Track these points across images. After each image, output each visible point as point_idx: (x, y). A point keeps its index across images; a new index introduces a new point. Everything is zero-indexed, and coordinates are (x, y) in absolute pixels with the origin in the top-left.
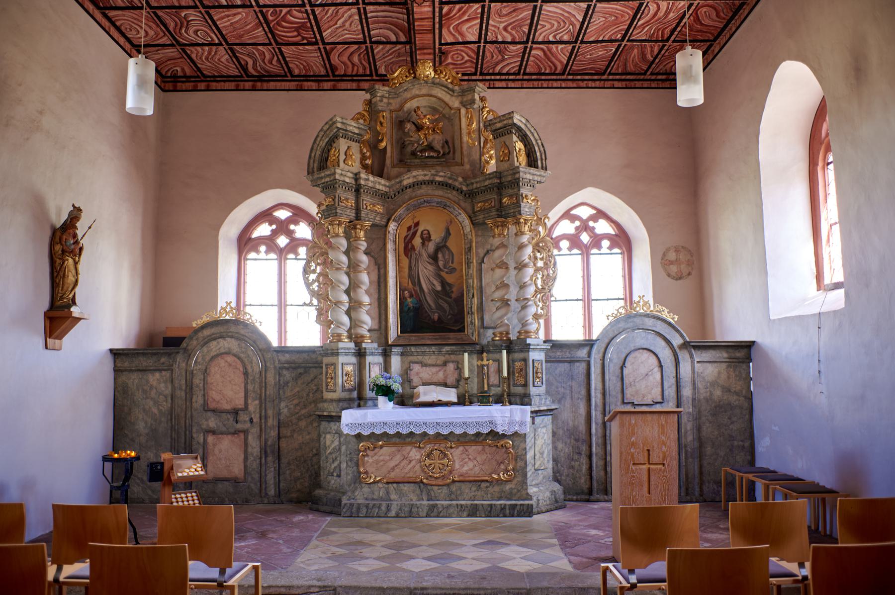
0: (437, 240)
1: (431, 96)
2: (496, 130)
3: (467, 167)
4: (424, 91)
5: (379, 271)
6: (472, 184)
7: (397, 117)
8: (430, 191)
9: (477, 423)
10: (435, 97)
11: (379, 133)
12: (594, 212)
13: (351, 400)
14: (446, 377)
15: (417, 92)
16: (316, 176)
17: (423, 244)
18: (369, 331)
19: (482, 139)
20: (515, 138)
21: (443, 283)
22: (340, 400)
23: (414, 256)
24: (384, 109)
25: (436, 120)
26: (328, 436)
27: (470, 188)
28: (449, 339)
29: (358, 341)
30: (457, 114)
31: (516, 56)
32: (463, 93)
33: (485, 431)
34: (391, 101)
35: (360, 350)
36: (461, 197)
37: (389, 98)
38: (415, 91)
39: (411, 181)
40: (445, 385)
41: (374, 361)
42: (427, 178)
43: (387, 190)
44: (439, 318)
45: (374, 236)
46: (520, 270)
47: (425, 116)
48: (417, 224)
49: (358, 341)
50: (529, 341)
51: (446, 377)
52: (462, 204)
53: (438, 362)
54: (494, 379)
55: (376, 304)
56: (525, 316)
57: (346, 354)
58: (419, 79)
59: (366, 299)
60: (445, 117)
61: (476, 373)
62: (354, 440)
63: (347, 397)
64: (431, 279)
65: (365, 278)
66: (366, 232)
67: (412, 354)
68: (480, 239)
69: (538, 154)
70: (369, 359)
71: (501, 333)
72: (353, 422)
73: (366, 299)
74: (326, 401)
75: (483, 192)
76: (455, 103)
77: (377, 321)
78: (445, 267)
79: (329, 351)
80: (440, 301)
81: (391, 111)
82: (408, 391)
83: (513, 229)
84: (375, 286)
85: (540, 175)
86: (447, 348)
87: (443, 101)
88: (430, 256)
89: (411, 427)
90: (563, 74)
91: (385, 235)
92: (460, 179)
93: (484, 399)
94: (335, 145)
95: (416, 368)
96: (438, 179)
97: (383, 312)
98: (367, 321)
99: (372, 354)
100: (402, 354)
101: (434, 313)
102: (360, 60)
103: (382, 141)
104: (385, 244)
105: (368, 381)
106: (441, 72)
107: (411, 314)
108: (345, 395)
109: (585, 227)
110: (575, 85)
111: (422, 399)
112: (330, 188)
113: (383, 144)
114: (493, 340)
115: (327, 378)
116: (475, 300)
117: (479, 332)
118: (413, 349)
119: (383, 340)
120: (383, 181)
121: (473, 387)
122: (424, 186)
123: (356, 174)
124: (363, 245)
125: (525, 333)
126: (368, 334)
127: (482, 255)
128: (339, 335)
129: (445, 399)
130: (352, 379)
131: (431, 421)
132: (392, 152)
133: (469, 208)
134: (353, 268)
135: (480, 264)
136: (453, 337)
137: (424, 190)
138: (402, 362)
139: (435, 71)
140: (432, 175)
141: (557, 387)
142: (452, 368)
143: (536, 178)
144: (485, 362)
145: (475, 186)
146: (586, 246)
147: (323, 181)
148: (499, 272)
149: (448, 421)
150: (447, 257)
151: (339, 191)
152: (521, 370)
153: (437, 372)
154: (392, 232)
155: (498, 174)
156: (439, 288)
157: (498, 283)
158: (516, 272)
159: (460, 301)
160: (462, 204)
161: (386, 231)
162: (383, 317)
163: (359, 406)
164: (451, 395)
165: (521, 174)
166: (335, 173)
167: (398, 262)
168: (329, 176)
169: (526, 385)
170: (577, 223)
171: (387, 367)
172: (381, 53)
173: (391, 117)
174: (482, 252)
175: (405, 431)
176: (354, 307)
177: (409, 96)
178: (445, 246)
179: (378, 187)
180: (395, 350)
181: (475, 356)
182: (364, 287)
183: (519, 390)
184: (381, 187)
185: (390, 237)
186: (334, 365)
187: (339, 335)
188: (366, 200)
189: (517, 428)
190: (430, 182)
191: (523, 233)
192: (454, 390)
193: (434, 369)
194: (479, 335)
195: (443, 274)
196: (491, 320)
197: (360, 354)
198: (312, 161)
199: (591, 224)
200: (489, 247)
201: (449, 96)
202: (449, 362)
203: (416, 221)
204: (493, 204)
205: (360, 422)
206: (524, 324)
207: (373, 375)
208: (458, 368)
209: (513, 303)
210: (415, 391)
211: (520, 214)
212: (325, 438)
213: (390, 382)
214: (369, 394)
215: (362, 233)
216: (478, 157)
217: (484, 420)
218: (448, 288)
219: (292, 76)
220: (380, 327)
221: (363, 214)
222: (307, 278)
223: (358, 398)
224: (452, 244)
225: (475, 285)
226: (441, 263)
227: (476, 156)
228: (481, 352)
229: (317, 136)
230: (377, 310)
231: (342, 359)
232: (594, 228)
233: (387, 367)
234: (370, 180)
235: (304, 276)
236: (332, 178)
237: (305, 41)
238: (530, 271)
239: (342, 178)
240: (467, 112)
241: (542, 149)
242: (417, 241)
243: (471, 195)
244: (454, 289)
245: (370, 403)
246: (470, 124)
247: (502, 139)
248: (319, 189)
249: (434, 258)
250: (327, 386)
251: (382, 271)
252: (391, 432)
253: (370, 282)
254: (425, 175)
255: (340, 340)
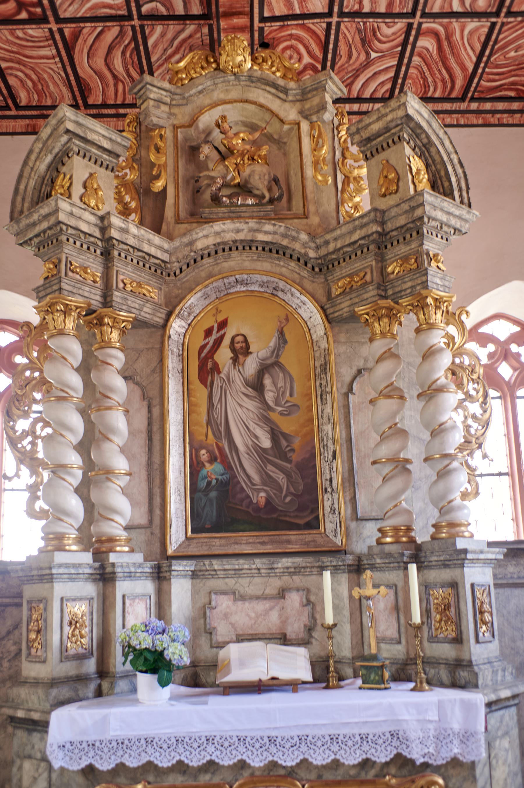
0: (263, 353)
1: (247, 101)
2: (369, 140)
3: (314, 220)
4: (234, 94)
5: (149, 407)
6: (327, 243)
7: (186, 140)
8: (247, 264)
9: (364, 738)
10: (254, 103)
11: (153, 165)
12: (517, 329)
13: (81, 679)
14: (284, 622)
15: (222, 96)
16: (24, 222)
17: (235, 360)
18: (127, 528)
19: (340, 178)
20: (408, 151)
21: (275, 434)
22: (54, 683)
23: (217, 382)
24: (161, 122)
25: (254, 143)
26: (27, 765)
27: (323, 251)
28: (289, 542)
29: (101, 549)
30: (295, 132)
31: (392, 56)
32: (304, 95)
33: (382, 757)
34: (175, 110)
35: (102, 567)
36: (305, 273)
37: (170, 106)
38: (218, 95)
39: (211, 241)
40: (284, 640)
41: (135, 595)
42: (241, 236)
43: (166, 257)
44: (268, 502)
45: (141, 346)
46: (431, 398)
47: (236, 134)
48: (223, 325)
49: (101, 549)
50: (460, 544)
51: (284, 622)
52: (307, 284)
53: (268, 591)
54: (387, 626)
55: (144, 475)
56: (448, 491)
57: (72, 578)
58: (224, 71)
59: (121, 464)
60: (271, 139)
61: (347, 613)
62: (80, 779)
63: (73, 672)
64: (252, 426)
65: (118, 420)
66: (123, 332)
67: (214, 574)
68: (342, 349)
69: (453, 179)
70: (122, 587)
71: (396, 529)
72: (77, 739)
73: (121, 464)
74: (24, 683)
75: (347, 257)
76: (291, 113)
77: (144, 508)
78: (277, 402)
79: (41, 572)
80: (270, 467)
81: (175, 128)
82: (206, 652)
83: (409, 320)
84: (142, 439)
85: (460, 217)
86: (286, 562)
87: (268, 110)
88: (247, 384)
89: (211, 749)
90: (462, 99)
91: (162, 343)
92: (304, 237)
93: (374, 674)
94: (64, 169)
95: (223, 603)
96: (261, 237)
97: (157, 491)
98: (122, 507)
99: (130, 576)
100: (194, 575)
101: (258, 491)
102: (125, 66)
103: (157, 177)
104: (162, 360)
105: (119, 634)
106: (264, 60)
107: (213, 494)
108: (69, 669)
109: (504, 353)
110: (481, 122)
111: (236, 675)
112: (48, 241)
113: (159, 185)
114: (379, 542)
115: (28, 631)
116: (339, 465)
117: (347, 529)
118: (216, 564)
119: (156, 547)
120: (157, 239)
121: (344, 645)
122: (234, 253)
123: (102, 218)
124: (117, 358)
125: (448, 527)
126: (123, 535)
127: (348, 379)
128: (60, 537)
129: (284, 674)
130: (85, 631)
131: (257, 734)
132: (177, 197)
133: (320, 293)
134: (94, 400)
135: (346, 395)
136: (296, 539)
137: (237, 260)
138: (195, 592)
139: (254, 60)
140: (251, 230)
141: (514, 641)
142: (297, 604)
143: (453, 222)
144: (370, 591)
145: (331, 247)
146: (508, 383)
147: (38, 229)
148: (386, 406)
149: (295, 733)
150: (281, 384)
151: (69, 250)
152: (447, 607)
153: (267, 612)
154: (175, 337)
155: (379, 215)
156: (266, 443)
157: (385, 427)
158: (420, 404)
159: (307, 468)
160: (307, 284)
161: (163, 335)
162: (157, 500)
163: (99, 693)
164: (296, 664)
165: (427, 208)
166: (56, 211)
167: (188, 393)
168: (46, 217)
169: (458, 640)
170: (491, 348)
171: (162, 607)
172: (161, 48)
173: (176, 137)
174: (347, 373)
175: (195, 761)
176: (94, 476)
177: (207, 101)
178: (277, 364)
179: (146, 248)
180: (178, 566)
181: (344, 578)
182: (119, 440)
183: (446, 651)
184: (153, 251)
185: (173, 348)
186: (45, 601)
187: (60, 537)
188: (125, 272)
189: (456, 750)
190: (248, 245)
191: (431, 326)
192: (302, 652)
193: (261, 606)
194: (348, 534)
195: (274, 416)
196: (365, 505)
197: (105, 577)
198: (19, 199)
199: (514, 348)
200: (361, 364)
201: (278, 102)
202: (290, 589)
203: (220, 319)
204: (368, 278)
205: (91, 738)
206: (445, 508)
207: (131, 621)
208: (309, 602)
209: (417, 467)
210: (222, 653)
211: (426, 287)
212: (20, 768)
213: (162, 642)
214: (119, 663)
215: (115, 335)
216: (333, 206)
217: (379, 730)
218: (284, 443)
219: (18, 107)
220: (151, 521)
221: (117, 296)
222: (13, 428)
223: (97, 677)
224: (288, 359)
225: (337, 436)
226: (269, 396)
227: (328, 205)
228: (357, 569)
229: (31, 152)
230: (144, 486)
231: (60, 589)
232: (519, 355)
233: (162, 607)
234: (131, 231)
235: (6, 423)
236: (52, 220)
237: (24, 15)
238: (453, 397)
239: (72, 222)
240: (312, 128)
241: (460, 171)
242: (224, 355)
243: (324, 267)
244: (297, 443)
245: (122, 685)
246: (316, 149)
247: (383, 156)
248: (29, 251)
249: (257, 386)
250: (29, 648)
251: (156, 411)
252: (164, 762)
253: (131, 433)
254: (238, 231)
255: (61, 549)
